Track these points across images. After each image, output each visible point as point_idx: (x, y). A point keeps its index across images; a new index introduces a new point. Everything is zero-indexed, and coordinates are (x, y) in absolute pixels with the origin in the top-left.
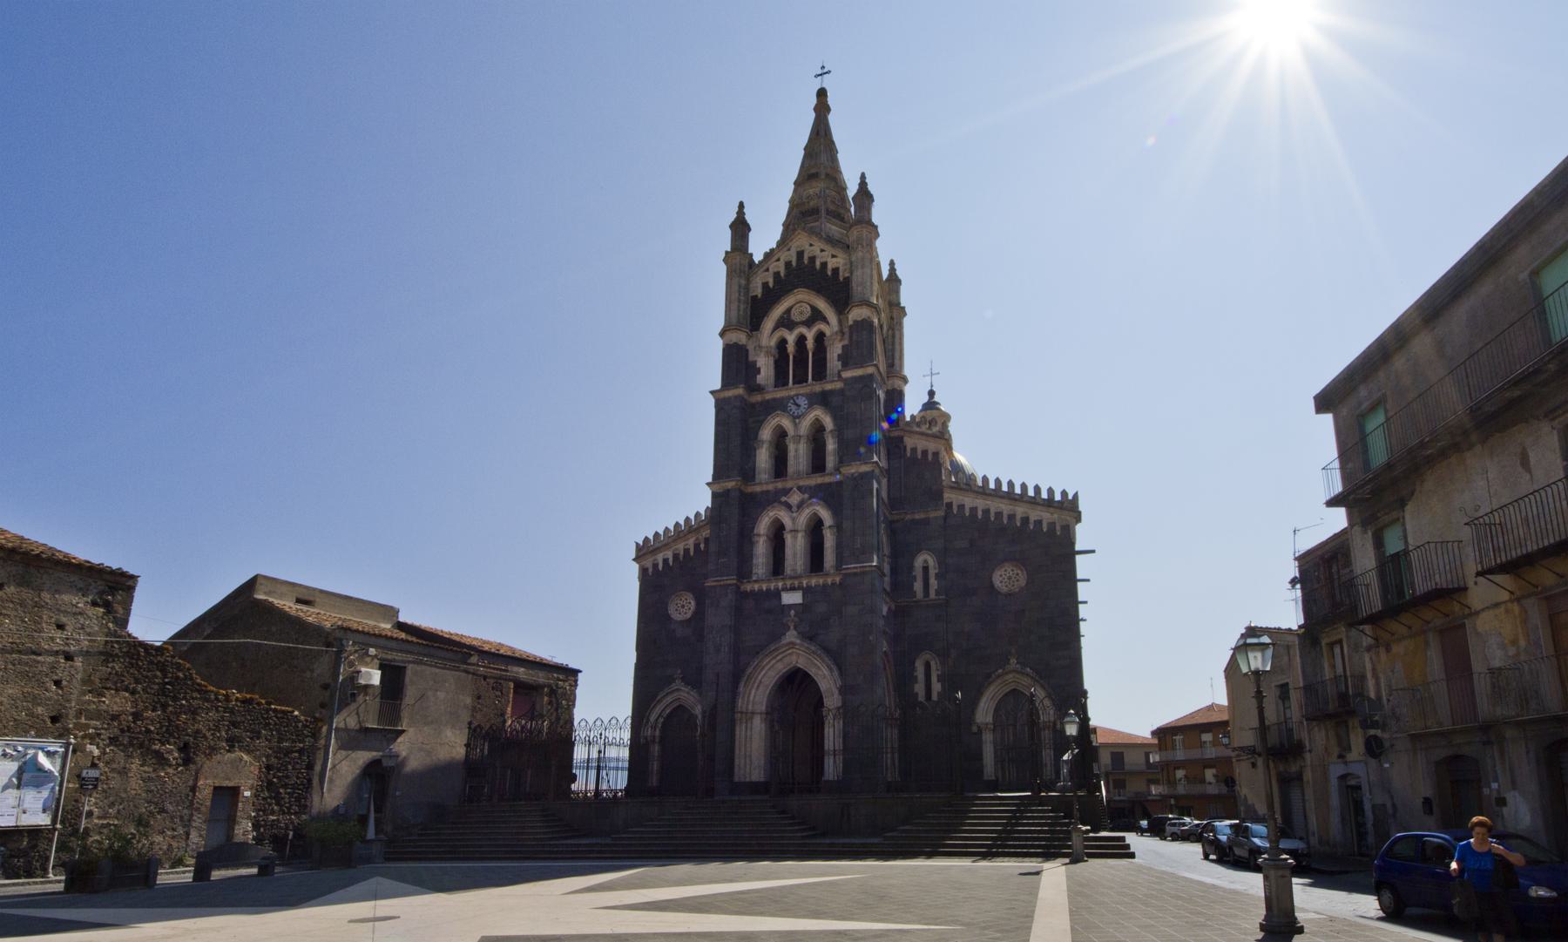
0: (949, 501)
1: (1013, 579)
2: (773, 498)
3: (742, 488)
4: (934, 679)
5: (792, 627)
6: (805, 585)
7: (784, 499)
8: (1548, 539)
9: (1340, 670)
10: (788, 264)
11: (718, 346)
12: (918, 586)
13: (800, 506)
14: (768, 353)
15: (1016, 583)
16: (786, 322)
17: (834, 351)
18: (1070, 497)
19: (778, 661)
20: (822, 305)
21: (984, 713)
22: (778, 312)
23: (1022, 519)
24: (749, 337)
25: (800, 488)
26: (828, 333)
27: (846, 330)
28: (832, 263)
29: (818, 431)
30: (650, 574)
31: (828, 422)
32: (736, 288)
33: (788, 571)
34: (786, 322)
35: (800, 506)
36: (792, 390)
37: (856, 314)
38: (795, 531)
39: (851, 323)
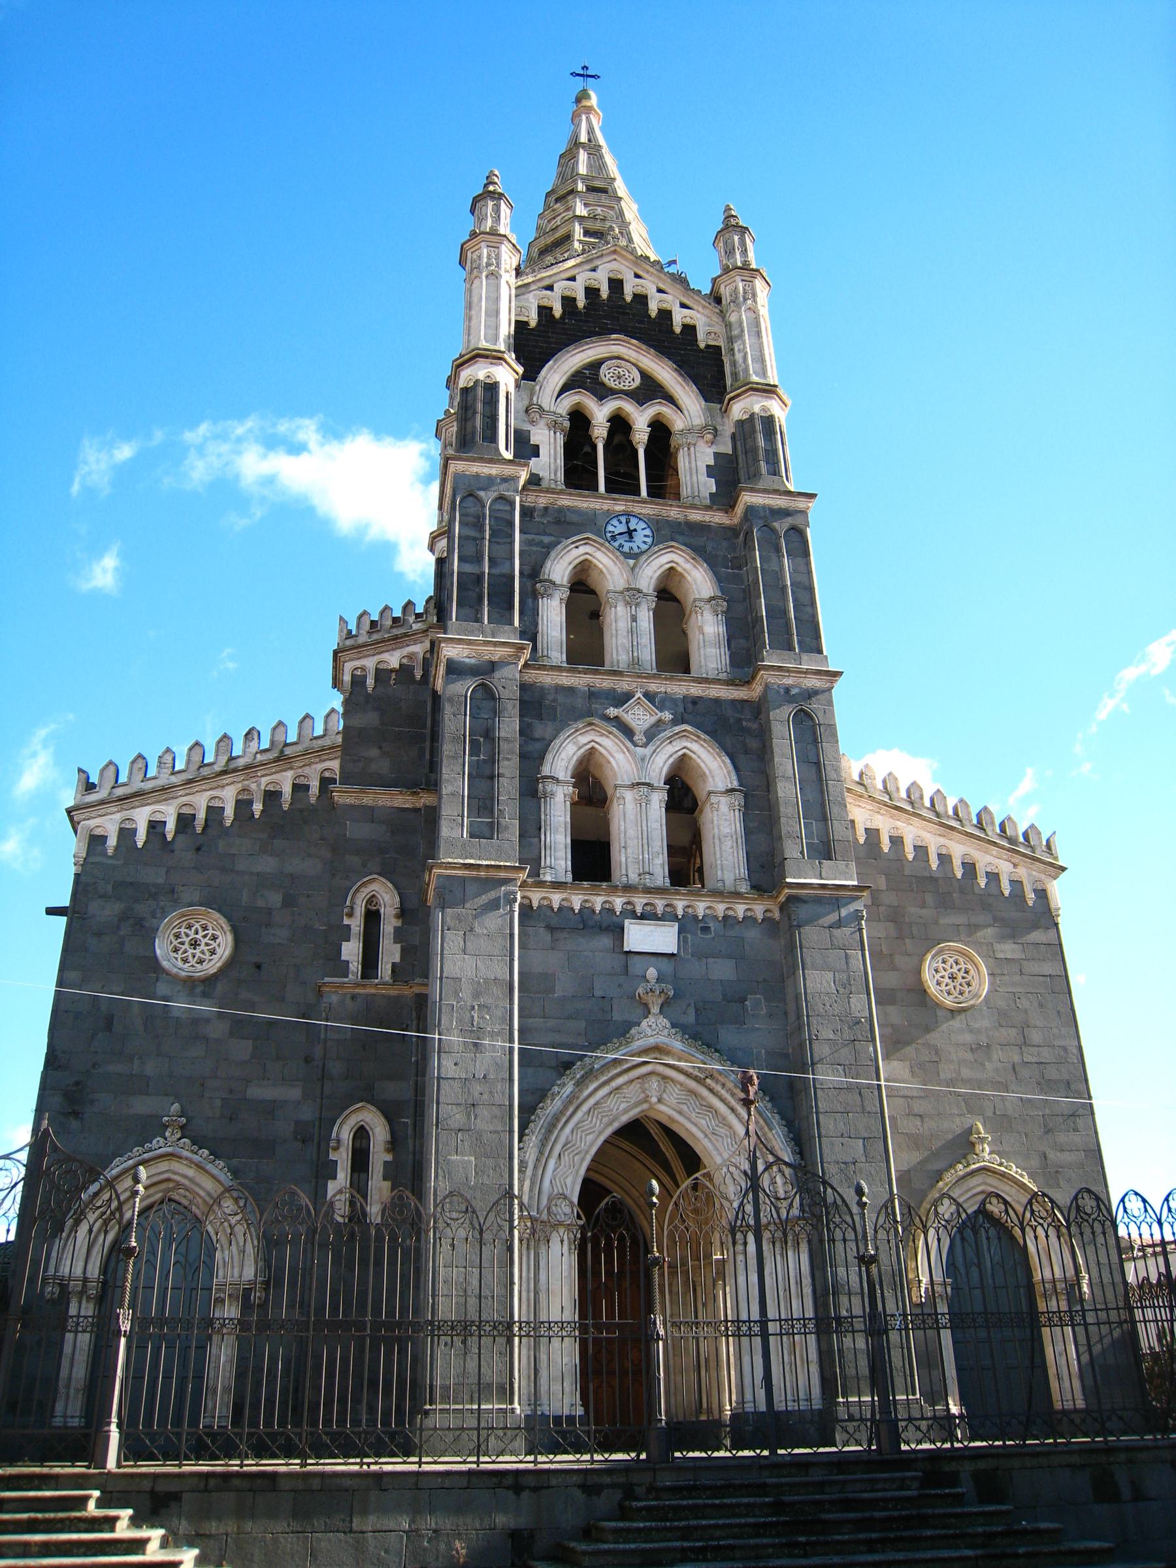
1: (960, 980)
5: (655, 1009)
6: (680, 913)
7: (612, 712)
8: (720, 1154)
13: (651, 734)
14: (554, 426)
15: (966, 989)
26: (678, 423)
30: (110, 852)
35: (651, 734)
36: (597, 503)
37: (738, 410)
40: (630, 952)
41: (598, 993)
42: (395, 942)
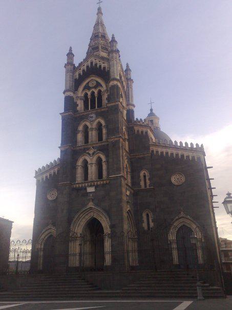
2: (84, 151)
4: (150, 221)
10: (87, 67)
11: (63, 97)
12: (142, 183)
14: (81, 99)
16: (87, 87)
17: (105, 97)
18: (200, 146)
20: (100, 80)
21: (172, 237)
22: (84, 84)
23: (171, 154)
24: (74, 93)
25: (93, 147)
26: (102, 91)
27: (109, 89)
28: (103, 66)
29: (100, 125)
31: (103, 123)
32: (68, 76)
33: (89, 179)
35: (93, 154)
37: (111, 83)
39: (110, 86)
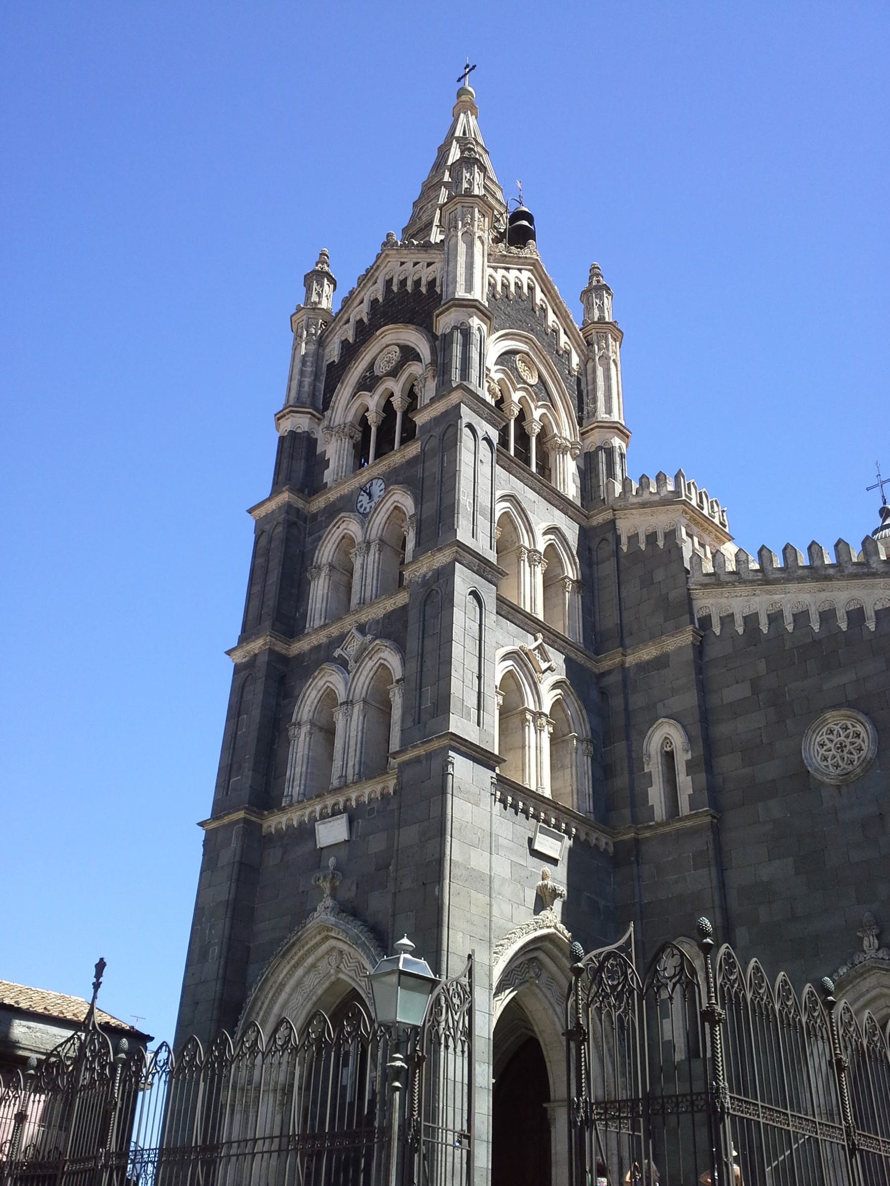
0: (704, 613)
3: (280, 647)
9: (32, 1095)
12: (656, 795)
16: (368, 383)
19: (308, 972)
34: (368, 383)
38: (349, 703)
40: (322, 849)
41: (301, 889)
42: (687, 775)
